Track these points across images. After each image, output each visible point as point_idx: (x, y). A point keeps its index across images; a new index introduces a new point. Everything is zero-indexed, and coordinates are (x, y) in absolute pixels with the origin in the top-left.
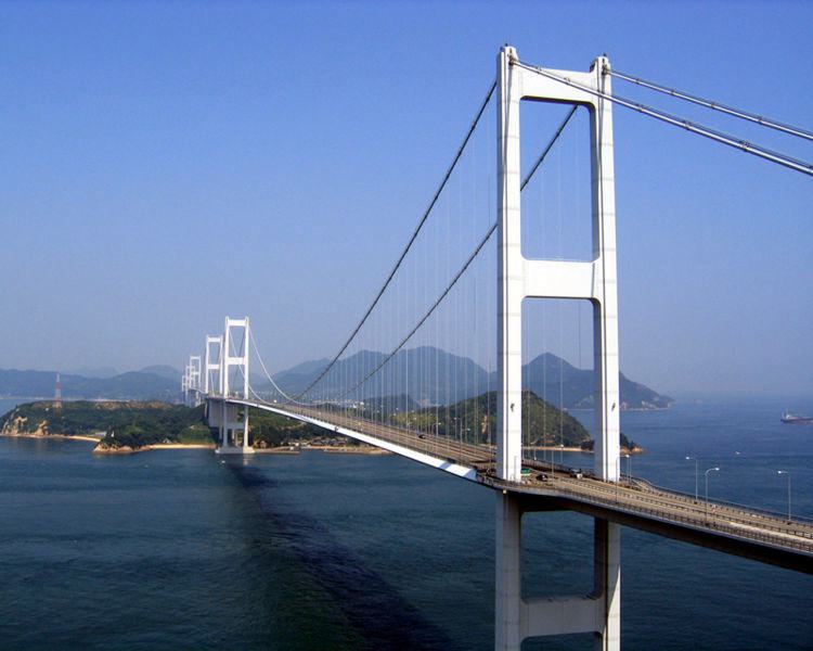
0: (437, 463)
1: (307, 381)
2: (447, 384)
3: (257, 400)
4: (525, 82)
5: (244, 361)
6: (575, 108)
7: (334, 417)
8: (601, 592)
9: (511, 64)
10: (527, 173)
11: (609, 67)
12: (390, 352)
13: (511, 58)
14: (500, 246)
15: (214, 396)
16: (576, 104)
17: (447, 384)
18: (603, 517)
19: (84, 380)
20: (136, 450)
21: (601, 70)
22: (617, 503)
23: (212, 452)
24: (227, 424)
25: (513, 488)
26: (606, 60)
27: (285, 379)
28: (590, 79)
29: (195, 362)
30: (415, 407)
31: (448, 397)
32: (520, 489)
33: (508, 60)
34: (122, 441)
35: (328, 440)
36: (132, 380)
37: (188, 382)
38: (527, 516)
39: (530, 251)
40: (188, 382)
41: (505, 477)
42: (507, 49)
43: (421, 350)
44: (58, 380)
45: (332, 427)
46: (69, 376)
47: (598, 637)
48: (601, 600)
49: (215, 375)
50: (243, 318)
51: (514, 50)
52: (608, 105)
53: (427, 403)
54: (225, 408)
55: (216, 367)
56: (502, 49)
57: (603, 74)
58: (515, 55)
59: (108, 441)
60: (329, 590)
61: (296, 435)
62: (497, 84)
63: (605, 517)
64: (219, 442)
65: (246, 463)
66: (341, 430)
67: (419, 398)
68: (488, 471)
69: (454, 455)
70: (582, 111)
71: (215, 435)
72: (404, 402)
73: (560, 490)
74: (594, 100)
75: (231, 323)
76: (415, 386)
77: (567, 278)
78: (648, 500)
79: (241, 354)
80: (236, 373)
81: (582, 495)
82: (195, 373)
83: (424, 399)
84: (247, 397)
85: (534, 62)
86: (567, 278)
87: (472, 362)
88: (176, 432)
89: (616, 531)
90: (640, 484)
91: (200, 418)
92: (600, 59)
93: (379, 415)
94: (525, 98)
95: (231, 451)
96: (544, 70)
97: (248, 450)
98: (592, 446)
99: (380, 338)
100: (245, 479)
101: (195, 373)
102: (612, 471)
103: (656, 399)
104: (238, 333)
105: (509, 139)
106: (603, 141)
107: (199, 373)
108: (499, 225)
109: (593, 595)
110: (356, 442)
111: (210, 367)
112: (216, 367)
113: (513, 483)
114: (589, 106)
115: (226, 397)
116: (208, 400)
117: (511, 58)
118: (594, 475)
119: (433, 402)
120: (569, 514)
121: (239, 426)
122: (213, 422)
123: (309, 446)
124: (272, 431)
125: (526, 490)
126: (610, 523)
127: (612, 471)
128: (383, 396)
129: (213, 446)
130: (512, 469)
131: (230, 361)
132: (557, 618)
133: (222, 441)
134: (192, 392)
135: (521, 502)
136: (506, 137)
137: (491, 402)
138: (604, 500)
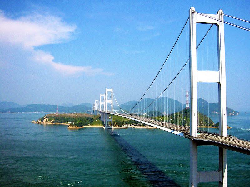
0: (170, 131)
1: (132, 106)
2: (171, 107)
3: (115, 113)
4: (197, 18)
5: (111, 101)
6: (212, 25)
7: (139, 118)
8: (221, 169)
9: (193, 13)
10: (198, 45)
11: (223, 13)
12: (157, 98)
13: (193, 11)
14: (190, 67)
15: (102, 112)
16: (212, 24)
17: (171, 107)
18: (221, 147)
19: (64, 107)
20: (81, 127)
21: (220, 14)
22: (227, 143)
23: (102, 128)
24: (106, 120)
25: (195, 138)
26: (222, 10)
27: (123, 106)
28: (217, 16)
29: (97, 102)
30: (161, 115)
31: (171, 112)
32: (197, 139)
33: (192, 11)
34: (76, 125)
35: (136, 124)
36: (76, 108)
37: (95, 108)
38: (199, 146)
39: (199, 68)
40: (95, 108)
41: (192, 135)
42: (192, 8)
43: (163, 98)
44: (57, 107)
45: (139, 121)
46: (60, 106)
47: (221, 183)
48: (220, 172)
49: (103, 106)
50: (111, 89)
51: (194, 8)
52: (223, 24)
53: (164, 113)
54: (106, 115)
55: (103, 103)
56: (191, 8)
57: (221, 15)
58: (194, 10)
59: (72, 125)
60: (163, 172)
61: (127, 123)
62: (189, 18)
63: (222, 147)
64: (104, 125)
65: (112, 131)
66: (141, 122)
67: (162, 112)
68: (187, 135)
69: (176, 128)
70: (215, 26)
71: (103, 123)
72: (157, 113)
73: (209, 139)
74: (218, 23)
75: (107, 90)
76: (161, 109)
77: (212, 76)
78: (234, 142)
79: (110, 100)
80: (109, 105)
81: (216, 141)
82: (97, 105)
83: (164, 112)
84: (112, 112)
85: (200, 11)
86: (212, 76)
87: (178, 101)
88: (92, 122)
89: (226, 151)
90: (233, 137)
91: (102, 118)
92: (220, 10)
93: (152, 115)
94: (198, 23)
95: (108, 128)
96: (203, 14)
97: (113, 128)
98: (218, 126)
99: (152, 95)
100: (113, 137)
101: (97, 105)
102: (224, 133)
103: (234, 112)
104: (109, 93)
105: (221, 37)
106: (222, 35)
107: (98, 105)
108: (190, 60)
109: (219, 170)
110: (145, 125)
111: (101, 103)
112: (103, 103)
113: (195, 137)
114: (217, 25)
115: (106, 112)
116: (100, 113)
117: (193, 11)
118: (219, 135)
119: (166, 113)
120: (212, 146)
121: (110, 120)
122: (102, 119)
123: (131, 126)
124: (120, 122)
125: (199, 139)
126: (224, 149)
127: (224, 133)
128: (171, 114)
129: (103, 126)
130: (195, 133)
131: (107, 101)
132: (210, 177)
133: (105, 125)
134: (96, 110)
135: (197, 143)
136: (220, 36)
137: (187, 112)
138: (223, 142)
